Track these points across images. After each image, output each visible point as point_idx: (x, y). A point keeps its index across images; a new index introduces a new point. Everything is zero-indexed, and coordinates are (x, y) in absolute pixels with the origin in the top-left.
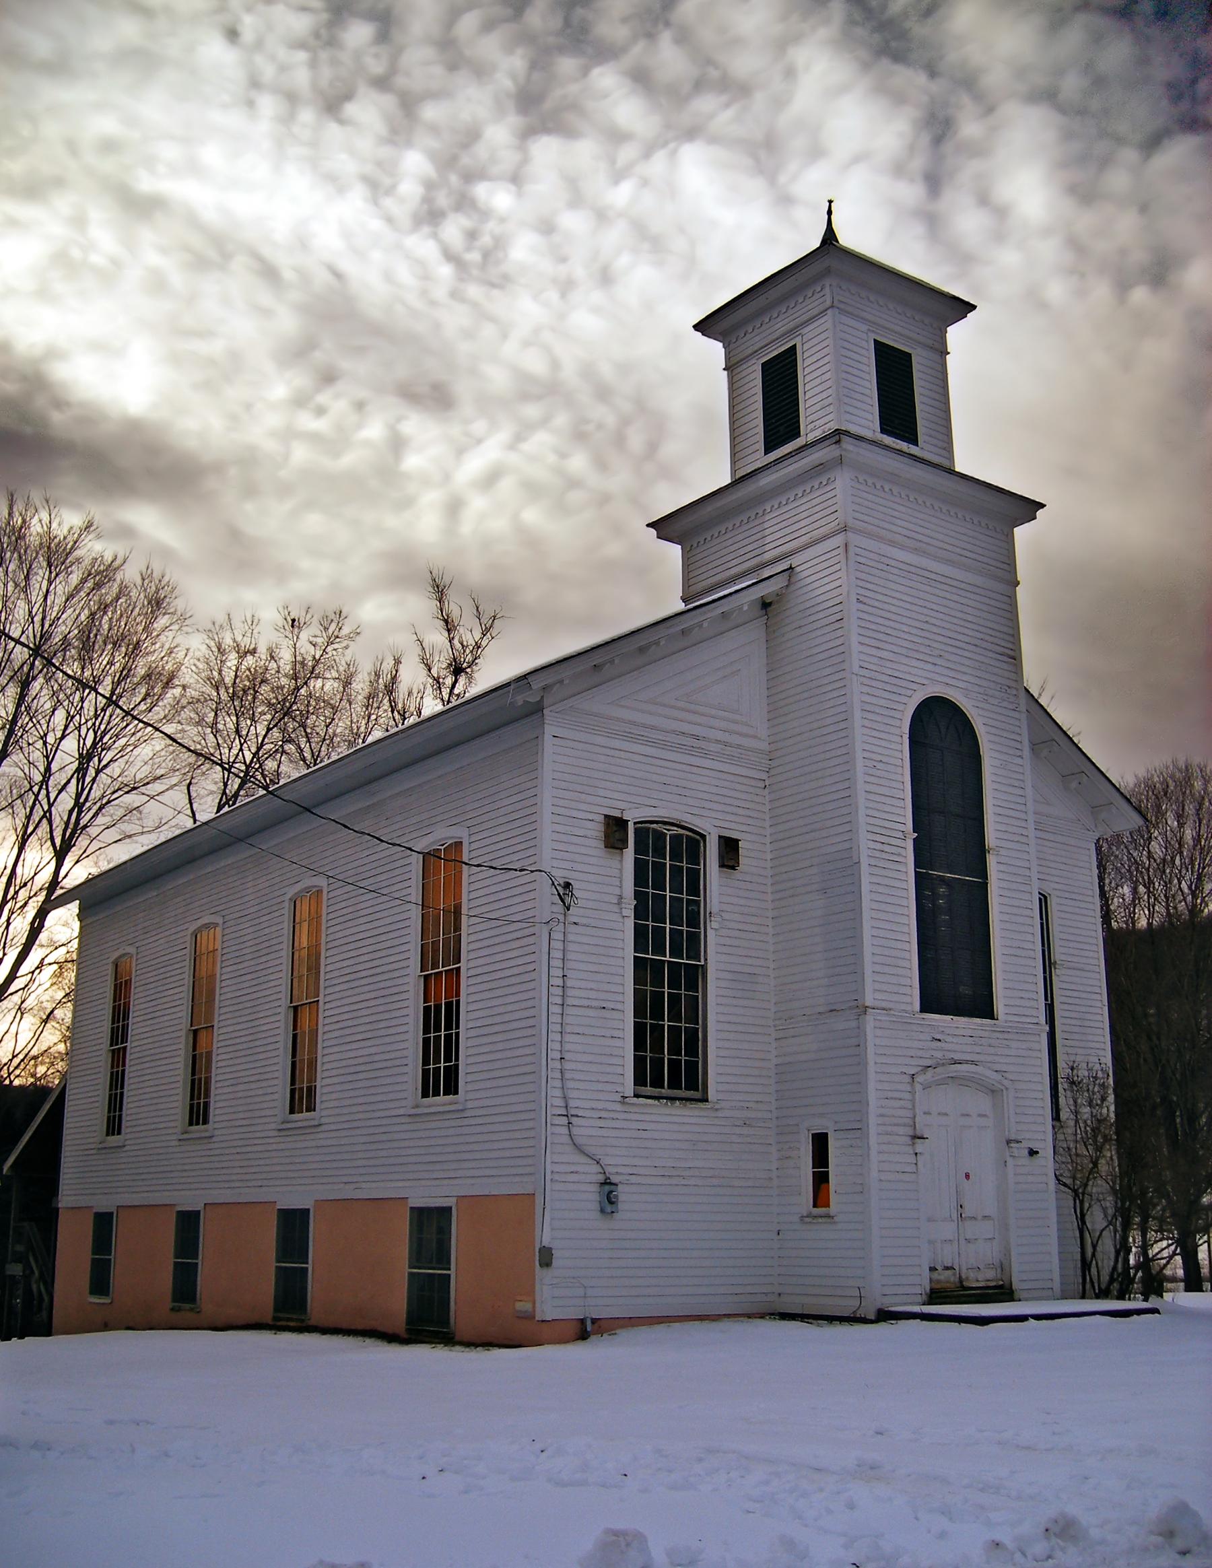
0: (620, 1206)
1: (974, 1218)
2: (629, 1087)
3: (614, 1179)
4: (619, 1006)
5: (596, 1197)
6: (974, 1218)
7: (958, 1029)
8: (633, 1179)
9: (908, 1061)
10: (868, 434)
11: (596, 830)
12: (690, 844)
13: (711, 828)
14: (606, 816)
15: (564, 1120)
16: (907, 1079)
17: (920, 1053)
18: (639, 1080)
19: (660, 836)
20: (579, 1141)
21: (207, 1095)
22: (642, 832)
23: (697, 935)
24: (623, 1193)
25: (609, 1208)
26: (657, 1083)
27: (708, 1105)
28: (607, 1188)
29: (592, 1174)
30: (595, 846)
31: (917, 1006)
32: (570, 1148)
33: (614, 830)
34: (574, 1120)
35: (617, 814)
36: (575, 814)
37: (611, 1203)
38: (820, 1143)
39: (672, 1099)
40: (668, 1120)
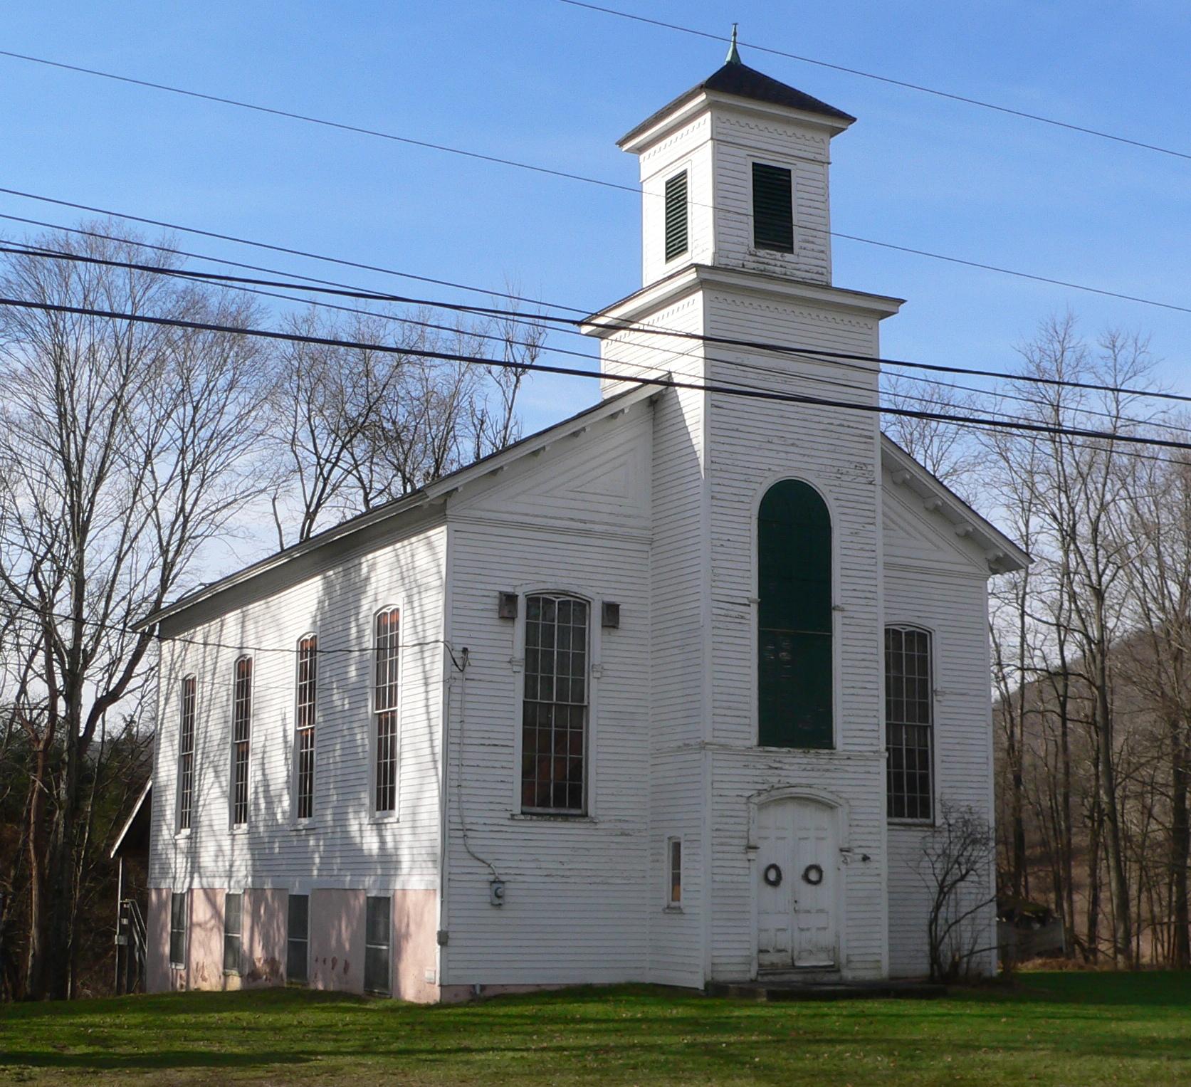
0: (507, 899)
1: (808, 912)
2: (517, 809)
3: (503, 878)
4: (510, 743)
5: (488, 892)
6: (808, 912)
7: (795, 766)
8: (520, 878)
9: (746, 786)
10: (800, 164)
11: (493, 603)
12: (575, 607)
13: (597, 592)
14: (500, 593)
15: (460, 834)
16: (744, 800)
17: (756, 779)
18: (527, 799)
19: (549, 602)
20: (472, 849)
21: (394, 730)
22: (532, 600)
23: (927, 775)
24: (510, 890)
25: (497, 901)
26: (544, 803)
27: (586, 819)
28: (496, 886)
29: (484, 874)
30: (490, 618)
31: (755, 741)
32: (467, 856)
33: (508, 601)
34: (469, 833)
35: (509, 590)
36: (474, 592)
37: (499, 897)
38: (677, 847)
39: (555, 816)
40: (554, 837)
